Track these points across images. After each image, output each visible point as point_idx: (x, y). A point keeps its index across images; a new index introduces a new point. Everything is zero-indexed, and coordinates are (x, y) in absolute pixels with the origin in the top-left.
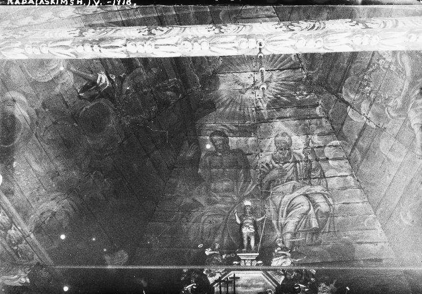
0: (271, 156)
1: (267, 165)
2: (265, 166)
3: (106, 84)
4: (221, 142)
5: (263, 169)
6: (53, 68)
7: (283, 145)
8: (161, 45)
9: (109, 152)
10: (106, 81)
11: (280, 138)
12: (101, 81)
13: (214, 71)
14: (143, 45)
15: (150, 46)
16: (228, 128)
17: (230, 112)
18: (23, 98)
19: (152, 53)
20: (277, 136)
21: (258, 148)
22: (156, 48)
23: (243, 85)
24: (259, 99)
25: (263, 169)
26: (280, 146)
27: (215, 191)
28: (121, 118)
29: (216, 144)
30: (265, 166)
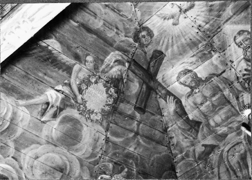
0: (243, 61)
1: (246, 70)
2: (245, 72)
3: (58, 97)
4: (190, 79)
5: (245, 77)
6: (5, 113)
7: (247, 43)
8: (34, 14)
9: (101, 153)
10: (57, 95)
11: (239, 39)
12: (52, 97)
13: (139, 24)
14: (19, 27)
15: (25, 23)
16: (187, 63)
17: (178, 47)
18: (205, 157)
19: (33, 28)
20: (235, 39)
21: (226, 63)
22: (32, 21)
23: (173, 17)
24: (195, 18)
25: (245, 77)
26: (245, 46)
27: (217, 125)
28: (90, 117)
29: (187, 84)
30: (245, 72)
